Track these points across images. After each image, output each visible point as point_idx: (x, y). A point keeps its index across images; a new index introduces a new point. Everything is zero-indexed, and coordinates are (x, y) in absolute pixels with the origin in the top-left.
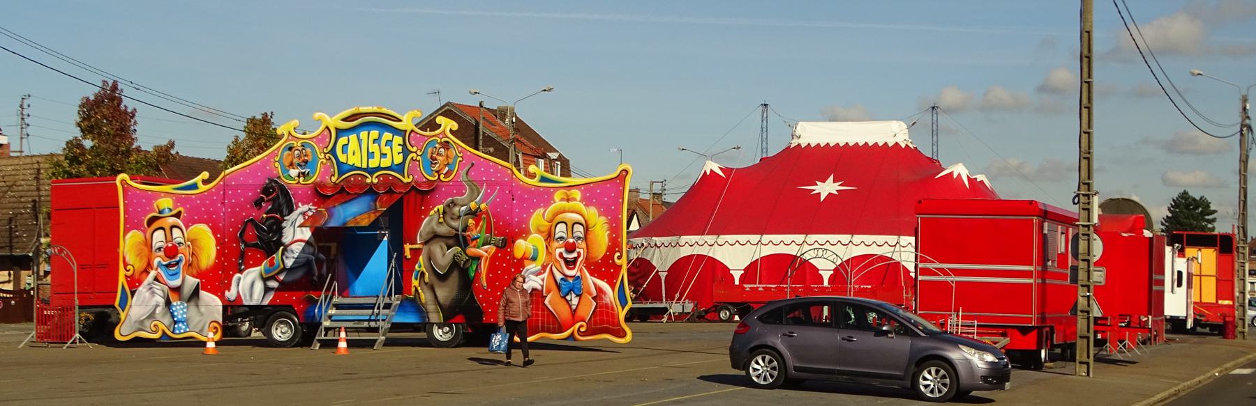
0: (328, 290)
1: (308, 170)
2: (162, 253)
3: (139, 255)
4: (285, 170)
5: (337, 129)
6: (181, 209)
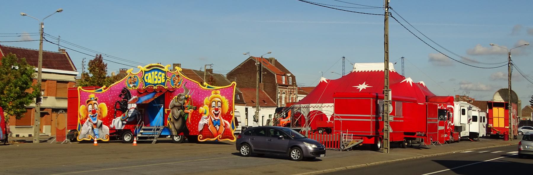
0: (140, 124)
1: (136, 85)
2: (91, 112)
3: (84, 113)
4: (129, 85)
5: (145, 71)
6: (97, 98)
